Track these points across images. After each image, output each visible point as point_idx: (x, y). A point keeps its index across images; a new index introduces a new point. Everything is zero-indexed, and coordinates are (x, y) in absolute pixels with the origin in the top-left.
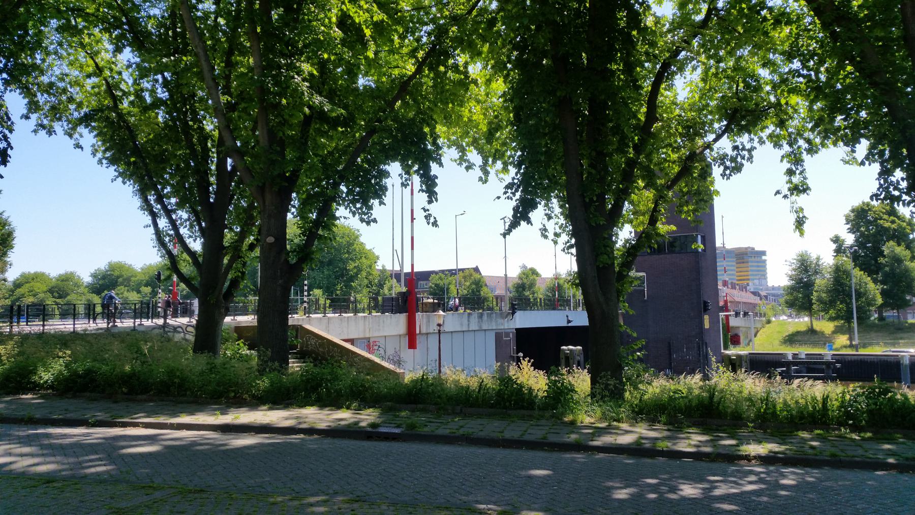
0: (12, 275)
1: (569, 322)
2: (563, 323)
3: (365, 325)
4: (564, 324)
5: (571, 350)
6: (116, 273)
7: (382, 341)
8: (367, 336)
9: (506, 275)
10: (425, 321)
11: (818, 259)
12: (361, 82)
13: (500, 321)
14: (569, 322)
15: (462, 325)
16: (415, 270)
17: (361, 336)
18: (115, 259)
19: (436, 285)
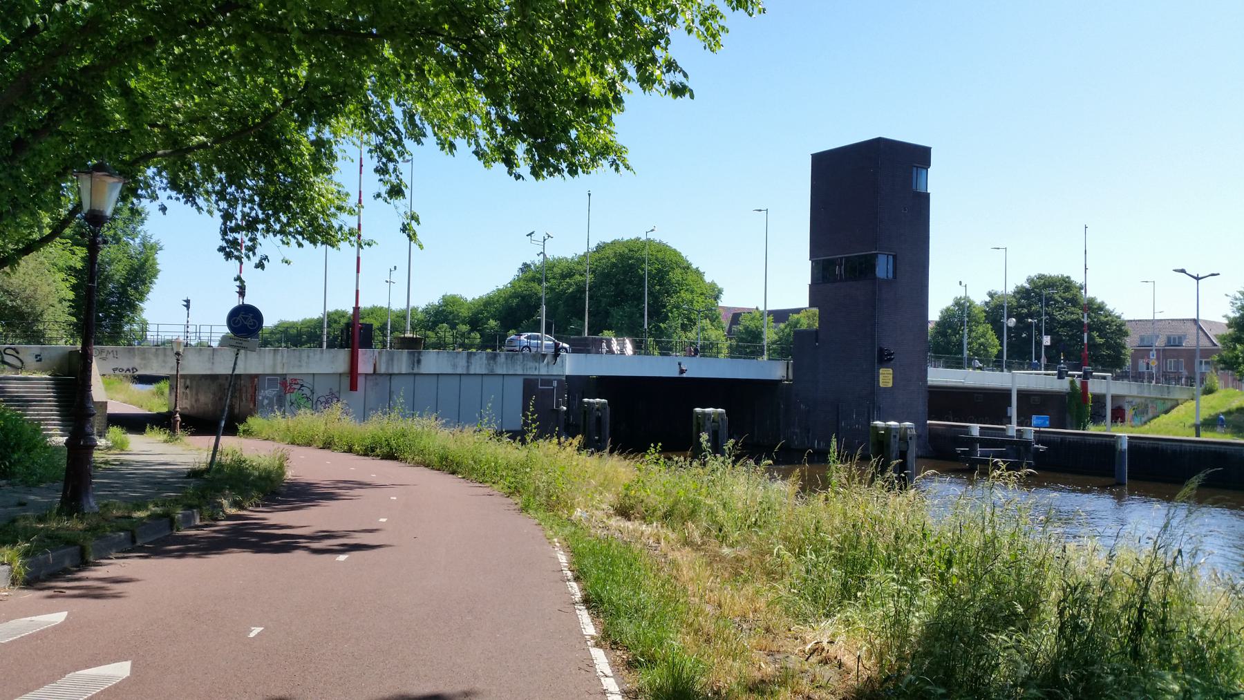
0: (934, 315)
1: (682, 371)
2: (674, 373)
3: (275, 359)
4: (676, 374)
5: (888, 429)
6: (450, 309)
7: (309, 380)
8: (279, 371)
9: (356, 309)
10: (384, 359)
11: (991, 295)
12: (590, 24)
13: (531, 364)
14: (682, 371)
15: (455, 366)
16: (412, 304)
17: (268, 371)
18: (1053, 269)
19: (746, 328)
